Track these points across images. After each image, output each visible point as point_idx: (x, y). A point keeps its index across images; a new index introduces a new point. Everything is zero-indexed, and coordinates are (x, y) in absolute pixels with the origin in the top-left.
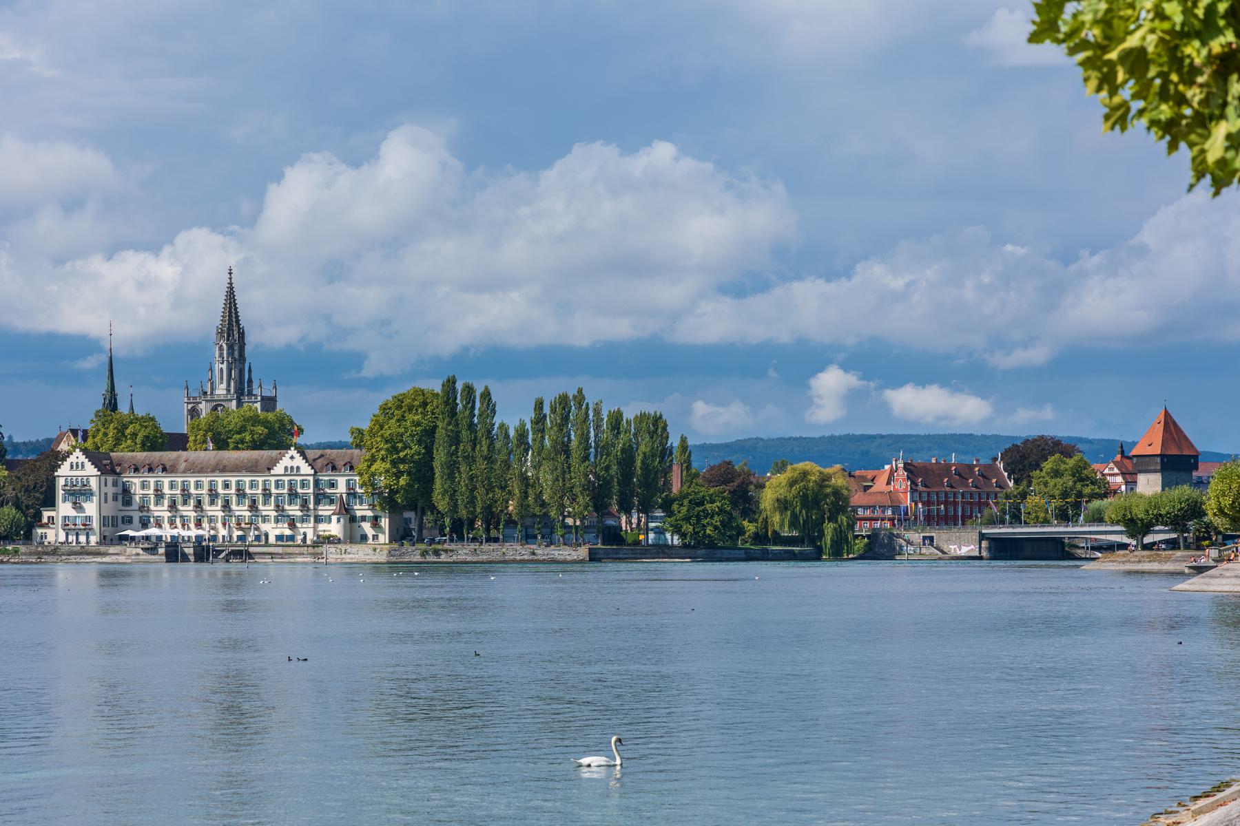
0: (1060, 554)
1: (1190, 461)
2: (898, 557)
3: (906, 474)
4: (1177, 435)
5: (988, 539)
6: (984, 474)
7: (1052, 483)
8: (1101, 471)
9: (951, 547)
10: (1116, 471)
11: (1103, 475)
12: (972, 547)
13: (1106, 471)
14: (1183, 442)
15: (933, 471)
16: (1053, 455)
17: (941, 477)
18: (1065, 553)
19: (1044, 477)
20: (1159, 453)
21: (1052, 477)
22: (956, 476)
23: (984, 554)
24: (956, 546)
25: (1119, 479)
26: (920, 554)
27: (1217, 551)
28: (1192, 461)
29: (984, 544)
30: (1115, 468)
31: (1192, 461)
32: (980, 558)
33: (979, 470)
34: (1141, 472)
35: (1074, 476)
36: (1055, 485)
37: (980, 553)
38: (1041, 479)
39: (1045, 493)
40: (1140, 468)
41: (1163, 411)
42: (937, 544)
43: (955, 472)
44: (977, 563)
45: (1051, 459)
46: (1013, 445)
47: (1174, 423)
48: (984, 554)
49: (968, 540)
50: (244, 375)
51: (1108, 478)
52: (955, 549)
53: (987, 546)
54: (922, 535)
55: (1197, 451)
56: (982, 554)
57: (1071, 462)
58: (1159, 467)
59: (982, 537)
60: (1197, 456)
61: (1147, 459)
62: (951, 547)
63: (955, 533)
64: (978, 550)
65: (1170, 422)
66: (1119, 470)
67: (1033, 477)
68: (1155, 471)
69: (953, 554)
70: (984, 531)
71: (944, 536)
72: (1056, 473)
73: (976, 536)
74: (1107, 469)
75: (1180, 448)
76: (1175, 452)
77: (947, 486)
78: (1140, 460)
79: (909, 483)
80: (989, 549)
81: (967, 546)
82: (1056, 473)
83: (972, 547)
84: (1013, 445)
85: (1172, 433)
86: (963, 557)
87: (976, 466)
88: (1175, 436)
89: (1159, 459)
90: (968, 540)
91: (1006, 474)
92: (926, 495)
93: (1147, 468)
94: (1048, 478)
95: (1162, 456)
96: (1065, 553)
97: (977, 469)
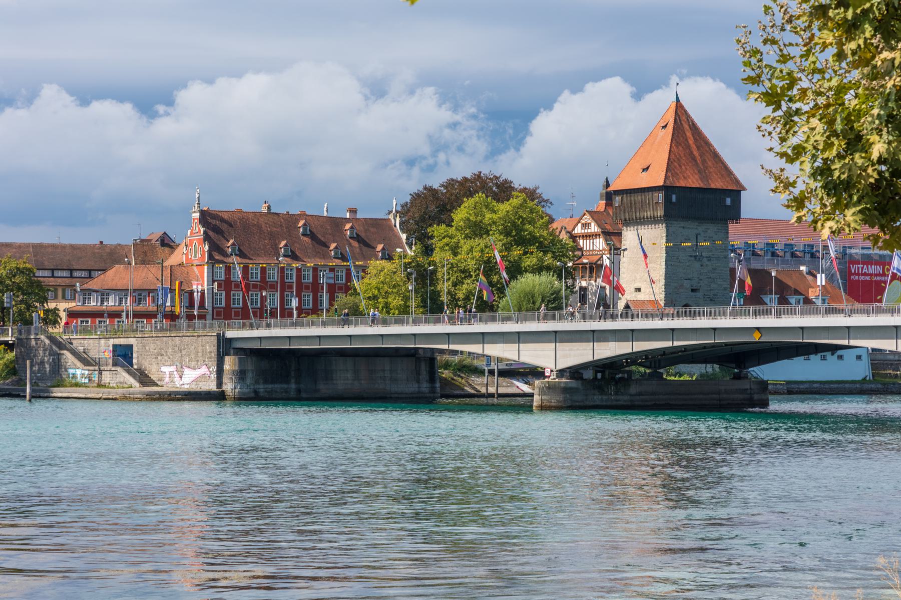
0: (425, 387)
1: (725, 201)
2: (58, 392)
3: (202, 229)
4: (698, 150)
5: (239, 351)
6: (363, 235)
7: (465, 246)
8: (570, 230)
9: (164, 369)
10: (594, 228)
11: (574, 238)
12: (204, 370)
13: (578, 230)
14: (710, 165)
15: (259, 227)
16: (472, 197)
17: (274, 239)
18: (438, 385)
19: (451, 237)
20: (661, 183)
21: (467, 237)
22: (305, 238)
23: (229, 386)
24: (173, 368)
25: (600, 244)
26: (99, 385)
27: (205, 366)
28: (728, 201)
29: (230, 363)
30: (593, 224)
31: (728, 201)
32: (218, 397)
33: (352, 228)
34: (628, 223)
35: (508, 234)
36: (471, 250)
37: (220, 384)
38: (446, 240)
39: (452, 267)
40: (627, 216)
41: (674, 99)
42: (138, 364)
43: (305, 229)
44: (209, 408)
45: (469, 203)
46: (425, 188)
47: (694, 128)
48: (229, 386)
49: (197, 353)
50: (686, 348)
51: (581, 242)
52: (171, 373)
53: (236, 368)
54: (112, 342)
55: (738, 182)
56: (224, 388)
57: (504, 208)
58: (660, 212)
59: (225, 346)
60: (738, 193)
61: (639, 197)
62: (164, 369)
63: (172, 342)
64: (214, 376)
65: (686, 126)
66: (599, 226)
67: (432, 237)
68: (654, 221)
69: (167, 386)
70: (230, 334)
71: (152, 346)
72: (477, 229)
73: (210, 346)
74: (580, 225)
75: (704, 174)
76: (694, 182)
77: (285, 256)
78: (627, 198)
79: (206, 248)
80: (241, 375)
81: (194, 369)
82: (477, 229)
83: (204, 370)
84: (425, 188)
85: (688, 146)
86: (177, 393)
87: (347, 221)
88: (695, 152)
89: (660, 197)
90: (197, 353)
91: (404, 236)
92: (223, 271)
93: (638, 215)
94: (459, 237)
95: (666, 189)
96: (438, 385)
97: (348, 226)
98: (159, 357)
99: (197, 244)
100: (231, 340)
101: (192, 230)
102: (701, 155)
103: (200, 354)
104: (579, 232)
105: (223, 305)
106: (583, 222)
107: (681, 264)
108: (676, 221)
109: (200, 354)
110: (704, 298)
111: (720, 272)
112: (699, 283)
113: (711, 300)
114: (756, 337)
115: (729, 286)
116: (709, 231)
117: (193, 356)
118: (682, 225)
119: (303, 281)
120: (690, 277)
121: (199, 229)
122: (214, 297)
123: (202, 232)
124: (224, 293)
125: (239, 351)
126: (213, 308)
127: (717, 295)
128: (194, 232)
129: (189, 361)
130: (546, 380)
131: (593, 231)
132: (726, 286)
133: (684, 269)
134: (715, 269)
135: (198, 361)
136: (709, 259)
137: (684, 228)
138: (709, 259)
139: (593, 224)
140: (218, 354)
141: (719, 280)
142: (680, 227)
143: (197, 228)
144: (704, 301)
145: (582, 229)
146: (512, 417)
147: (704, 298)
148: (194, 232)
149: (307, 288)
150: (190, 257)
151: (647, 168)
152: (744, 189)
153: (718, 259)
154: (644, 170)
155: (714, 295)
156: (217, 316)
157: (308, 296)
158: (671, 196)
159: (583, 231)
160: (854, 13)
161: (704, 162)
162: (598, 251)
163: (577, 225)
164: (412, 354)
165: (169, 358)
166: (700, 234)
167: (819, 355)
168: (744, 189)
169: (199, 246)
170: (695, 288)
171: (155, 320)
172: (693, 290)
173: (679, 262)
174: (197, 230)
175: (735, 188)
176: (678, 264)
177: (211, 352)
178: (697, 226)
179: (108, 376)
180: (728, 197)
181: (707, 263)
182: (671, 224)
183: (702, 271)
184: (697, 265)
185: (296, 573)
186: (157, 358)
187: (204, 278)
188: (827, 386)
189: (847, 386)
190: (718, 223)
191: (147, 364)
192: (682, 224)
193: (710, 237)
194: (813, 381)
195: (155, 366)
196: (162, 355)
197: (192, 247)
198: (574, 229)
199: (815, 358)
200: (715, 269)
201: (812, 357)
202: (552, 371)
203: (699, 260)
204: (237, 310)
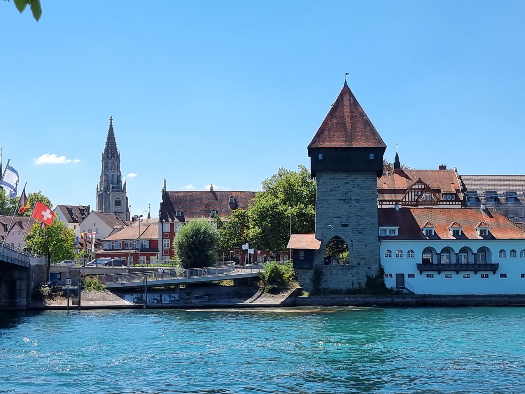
47: (355, 103)
102: (352, 124)
107: (331, 206)
108: (326, 174)
110: (353, 231)
111: (367, 211)
112: (348, 220)
116: (358, 180)
118: (333, 177)
120: (339, 215)
126: (162, 249)
127: (365, 229)
132: (373, 222)
133: (334, 210)
134: (363, 209)
136: (357, 201)
137: (333, 178)
138: (357, 201)
141: (367, 217)
142: (330, 178)
144: (352, 233)
147: (353, 231)
153: (366, 201)
155: (362, 229)
156: (165, 254)
161: (353, 128)
173: (329, 204)
176: (329, 206)
178: (346, 177)
180: (372, 153)
181: (355, 204)
182: (322, 176)
184: (347, 206)
185: (413, 370)
188: (471, 299)
189: (493, 299)
190: (367, 174)
192: (332, 176)
194: (473, 295)
200: (363, 209)
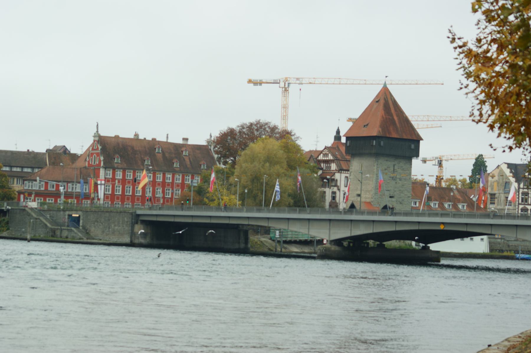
5: (143, 222)
28: (413, 146)
30: (330, 155)
51: (322, 165)
60: (418, 142)
74: (322, 155)
98: (96, 223)
99: (96, 156)
100: (139, 215)
101: (93, 147)
103: (121, 223)
104: (321, 159)
105: (131, 194)
106: (324, 153)
109: (121, 223)
112: (394, 193)
113: (401, 203)
114: (442, 227)
115: (411, 195)
117: (116, 223)
119: (126, 178)
120: (389, 189)
121: (98, 147)
122: (105, 188)
123: (100, 149)
124: (121, 186)
125: (143, 222)
128: (94, 148)
129: (114, 226)
130: (324, 246)
131: (330, 159)
132: (409, 195)
135: (119, 226)
139: (330, 155)
140: (132, 223)
143: (96, 147)
145: (323, 157)
146: (379, 266)
148: (94, 148)
149: (159, 184)
150: (91, 163)
151: (367, 125)
152: (422, 139)
153: (405, 180)
154: (365, 126)
157: (130, 187)
158: (380, 142)
159: (323, 158)
160: (508, 48)
162: (332, 171)
163: (320, 154)
164: (236, 227)
165: (102, 224)
166: (395, 165)
167: (469, 238)
168: (422, 139)
169: (97, 157)
170: (392, 196)
171: (60, 199)
172: (391, 197)
174: (96, 148)
175: (415, 139)
177: (127, 222)
179: (66, 232)
183: (396, 186)
186: (94, 223)
187: (424, 202)
191: (88, 226)
193: (401, 167)
195: (93, 228)
196: (97, 222)
197: (92, 157)
198: (318, 157)
199: (467, 240)
201: (465, 239)
202: (327, 241)
203: (395, 180)
204: (119, 196)
